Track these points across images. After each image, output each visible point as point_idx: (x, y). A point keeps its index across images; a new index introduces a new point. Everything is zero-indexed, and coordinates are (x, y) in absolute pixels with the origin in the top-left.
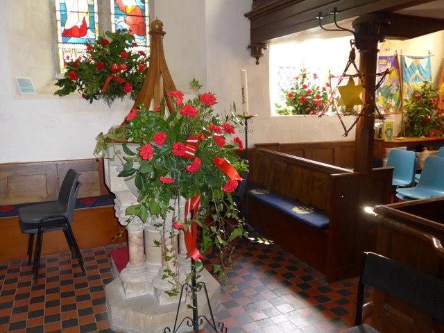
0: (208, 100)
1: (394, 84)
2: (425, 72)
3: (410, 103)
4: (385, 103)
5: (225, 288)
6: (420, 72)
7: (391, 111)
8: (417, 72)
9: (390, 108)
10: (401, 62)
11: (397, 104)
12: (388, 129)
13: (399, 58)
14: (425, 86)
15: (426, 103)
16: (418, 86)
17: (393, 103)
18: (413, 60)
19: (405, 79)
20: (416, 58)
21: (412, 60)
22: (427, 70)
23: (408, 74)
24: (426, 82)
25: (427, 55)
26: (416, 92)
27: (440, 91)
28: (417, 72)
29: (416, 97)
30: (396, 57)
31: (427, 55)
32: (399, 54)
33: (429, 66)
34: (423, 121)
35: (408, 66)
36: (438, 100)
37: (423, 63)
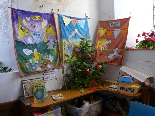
0: (144, 34)
1: (51, 41)
2: (84, 31)
3: (71, 57)
4: (42, 59)
5: (147, 79)
6: (79, 31)
7: (49, 66)
8: (76, 30)
9: (47, 63)
10: (59, 20)
11: (55, 60)
12: (37, 90)
13: (56, 17)
14: (82, 42)
15: (85, 58)
16: (77, 42)
17: (51, 59)
18: (70, 20)
19: (64, 36)
20: (74, 18)
21: (70, 20)
22: (86, 30)
23: (67, 32)
24: (83, 39)
25: (85, 17)
26: (76, 48)
27: (98, 47)
28: (76, 30)
29: (75, 51)
30: (52, 15)
31: (85, 17)
32: (55, 12)
33: (86, 26)
34: (83, 75)
35: (66, 24)
36: (96, 53)
37: (82, 24)
